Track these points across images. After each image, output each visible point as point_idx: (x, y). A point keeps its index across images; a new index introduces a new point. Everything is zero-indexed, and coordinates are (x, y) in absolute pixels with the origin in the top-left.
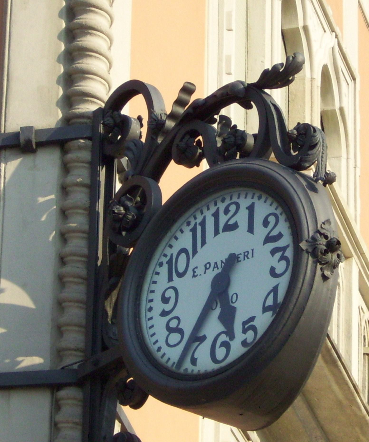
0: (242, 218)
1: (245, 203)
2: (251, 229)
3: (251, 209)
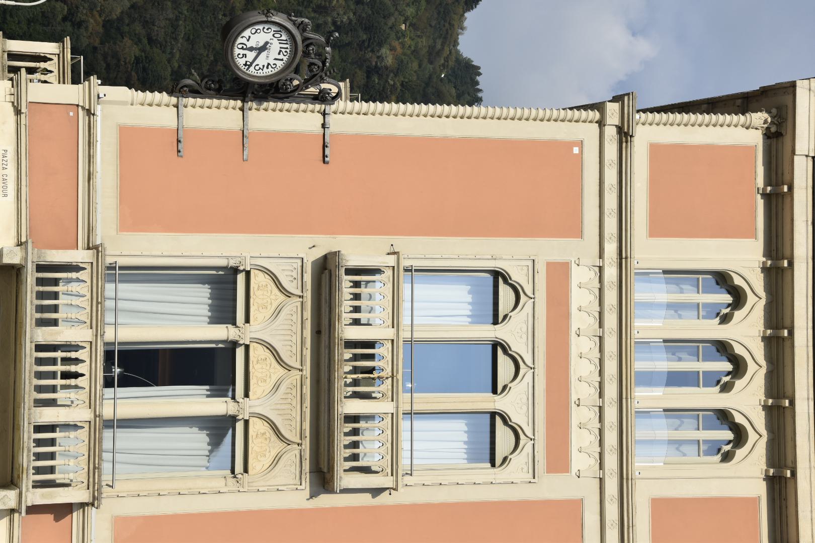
0: (281, 57)
1: (285, 58)
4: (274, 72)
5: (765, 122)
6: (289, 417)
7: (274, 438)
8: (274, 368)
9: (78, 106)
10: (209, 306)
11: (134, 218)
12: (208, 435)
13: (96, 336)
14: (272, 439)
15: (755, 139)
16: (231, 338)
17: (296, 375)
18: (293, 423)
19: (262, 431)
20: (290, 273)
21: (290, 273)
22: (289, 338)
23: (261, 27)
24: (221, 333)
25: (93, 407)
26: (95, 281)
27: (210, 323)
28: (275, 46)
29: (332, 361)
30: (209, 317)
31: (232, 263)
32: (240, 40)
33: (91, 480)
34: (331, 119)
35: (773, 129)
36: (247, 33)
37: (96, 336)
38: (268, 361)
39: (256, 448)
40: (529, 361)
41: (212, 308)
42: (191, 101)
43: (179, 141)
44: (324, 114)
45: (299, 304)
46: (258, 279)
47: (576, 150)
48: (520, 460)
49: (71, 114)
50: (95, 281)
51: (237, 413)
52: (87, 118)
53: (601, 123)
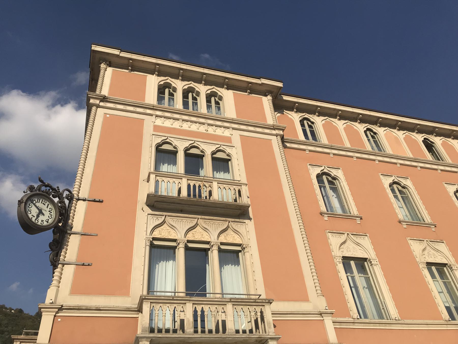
1: (48, 203)
2: (47, 207)
3: (48, 205)
4: (54, 210)
5: (104, 64)
7: (226, 232)
9: (55, 316)
11: (124, 289)
13: (190, 300)
15: (110, 70)
17: (200, 221)
18: (221, 224)
20: (155, 220)
21: (155, 220)
22: (184, 223)
23: (28, 209)
24: (181, 253)
25: (226, 303)
26: (161, 301)
28: (39, 205)
29: (195, 206)
32: (33, 219)
33: (260, 304)
34: (81, 196)
35: (108, 63)
36: (30, 216)
37: (190, 300)
39: (231, 240)
40: (193, 142)
42: (62, 257)
43: (83, 265)
44: (78, 199)
45: (169, 217)
46: (156, 234)
47: (108, 116)
48: (228, 150)
49: (59, 320)
50: (161, 301)
52: (64, 311)
53: (98, 106)
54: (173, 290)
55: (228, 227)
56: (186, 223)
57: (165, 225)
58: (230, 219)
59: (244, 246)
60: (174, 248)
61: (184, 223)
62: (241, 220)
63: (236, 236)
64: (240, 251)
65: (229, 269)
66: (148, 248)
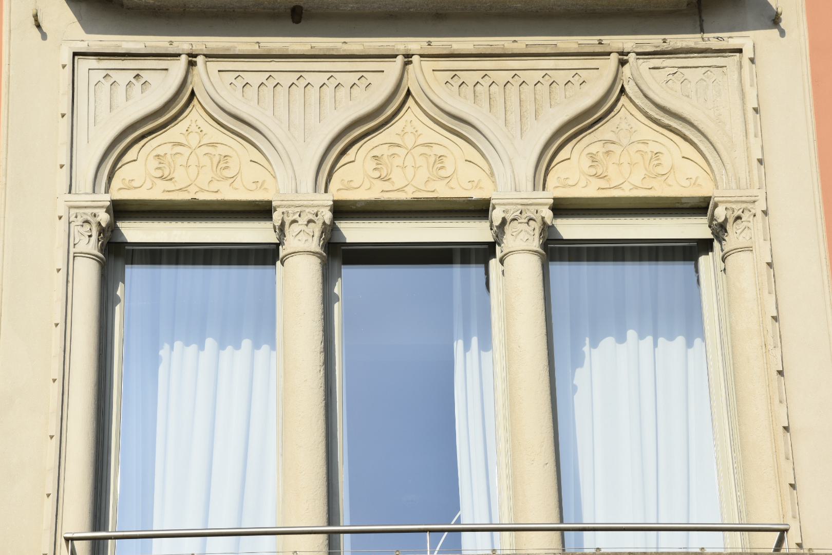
6: (543, 89)
7: (604, 131)
8: (404, 133)
10: (222, 346)
12: (594, 345)
14: (609, 136)
16: (315, 245)
19: (586, 162)
20: (121, 90)
21: (121, 90)
22: (313, 92)
27: (272, 343)
30: (257, 346)
31: (90, 245)
38: (384, 151)
39: (637, 178)
41: (229, 337)
45: (215, 66)
46: (139, 180)
51: (537, 226)
54: (548, 517)
55: (617, 92)
56: (328, 91)
57: (194, 116)
58: (627, 42)
59: (720, 214)
60: (481, 254)
61: (313, 92)
62: (711, 40)
63: (673, 150)
64: (705, 246)
65: (620, 372)
66: (87, 273)
